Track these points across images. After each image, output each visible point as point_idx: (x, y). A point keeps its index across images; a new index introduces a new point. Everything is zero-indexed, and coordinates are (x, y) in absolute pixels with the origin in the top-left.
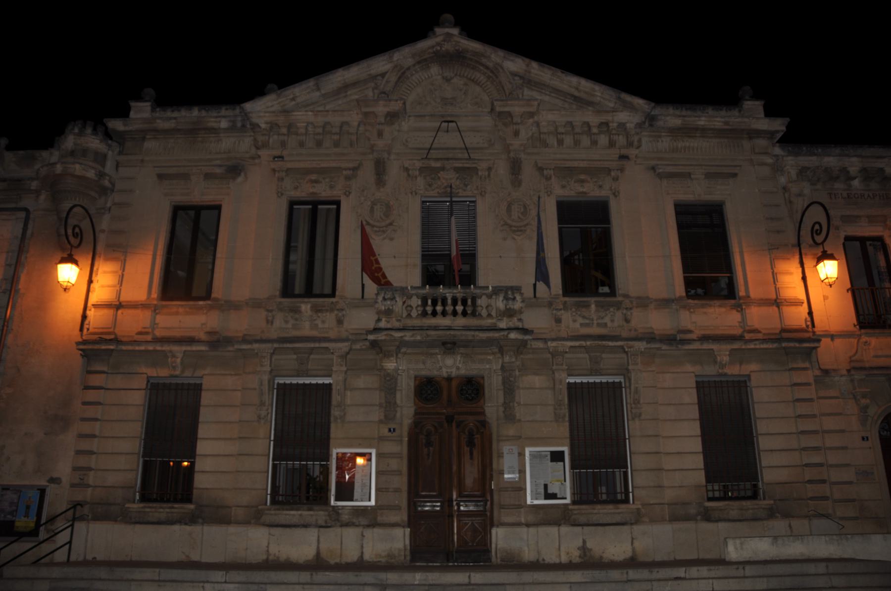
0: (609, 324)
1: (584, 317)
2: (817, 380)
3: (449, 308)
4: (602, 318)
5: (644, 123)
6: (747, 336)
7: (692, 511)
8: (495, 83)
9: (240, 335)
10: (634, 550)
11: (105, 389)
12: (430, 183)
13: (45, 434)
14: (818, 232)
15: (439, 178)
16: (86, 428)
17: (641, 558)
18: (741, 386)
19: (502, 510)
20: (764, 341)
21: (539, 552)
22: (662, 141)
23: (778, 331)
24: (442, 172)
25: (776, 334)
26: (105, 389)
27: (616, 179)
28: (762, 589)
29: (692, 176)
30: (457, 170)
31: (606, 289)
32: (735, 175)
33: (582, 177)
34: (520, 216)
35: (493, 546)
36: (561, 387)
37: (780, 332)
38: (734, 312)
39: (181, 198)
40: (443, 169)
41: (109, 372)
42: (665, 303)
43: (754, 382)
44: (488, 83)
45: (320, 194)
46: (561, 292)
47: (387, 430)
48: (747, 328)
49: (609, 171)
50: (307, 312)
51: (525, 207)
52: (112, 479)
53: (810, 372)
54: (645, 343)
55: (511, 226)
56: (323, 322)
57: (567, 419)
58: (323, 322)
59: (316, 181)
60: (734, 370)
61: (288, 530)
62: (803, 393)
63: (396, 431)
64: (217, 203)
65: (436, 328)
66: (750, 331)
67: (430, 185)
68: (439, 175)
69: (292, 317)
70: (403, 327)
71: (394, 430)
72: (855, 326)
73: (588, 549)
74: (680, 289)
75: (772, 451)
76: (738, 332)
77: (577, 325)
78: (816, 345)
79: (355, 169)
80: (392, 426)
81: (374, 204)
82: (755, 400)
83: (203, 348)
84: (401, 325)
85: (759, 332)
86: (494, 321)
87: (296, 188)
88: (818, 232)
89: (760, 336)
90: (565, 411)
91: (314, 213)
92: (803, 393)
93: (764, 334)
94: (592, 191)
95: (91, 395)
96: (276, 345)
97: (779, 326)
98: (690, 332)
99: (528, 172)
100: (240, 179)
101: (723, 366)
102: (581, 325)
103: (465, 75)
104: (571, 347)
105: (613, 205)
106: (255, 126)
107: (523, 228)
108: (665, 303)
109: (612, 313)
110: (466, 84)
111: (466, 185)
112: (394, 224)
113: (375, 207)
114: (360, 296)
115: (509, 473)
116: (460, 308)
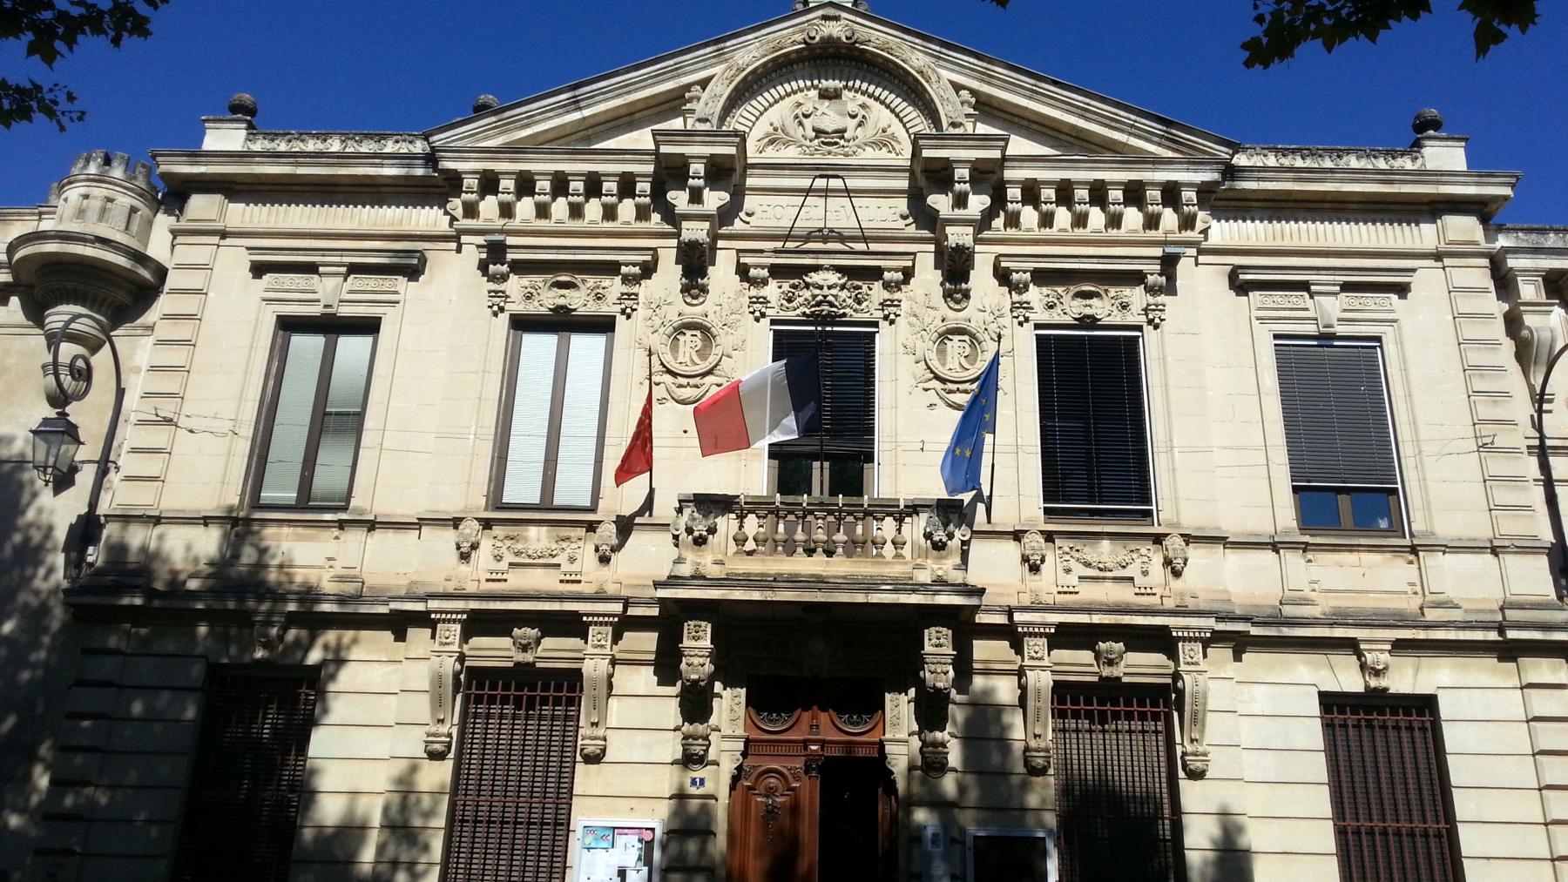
0: (1139, 580)
1: (1088, 565)
6: (1432, 615)
9: (404, 582)
12: (790, 294)
28: (1551, 577)
30: (838, 269)
31: (1383, 524)
37: (1502, 609)
40: (816, 268)
46: (1295, 524)
48: (1429, 598)
50: (539, 540)
58: (572, 560)
63: (689, 781)
67: (790, 300)
68: (807, 279)
70: (727, 574)
74: (1286, 516)
75: (1488, 858)
76: (1411, 604)
80: (698, 775)
84: (724, 573)
85: (1458, 607)
86: (907, 569)
89: (1456, 615)
91: (198, 292)
93: (1466, 611)
97: (1499, 596)
98: (1306, 602)
99: (981, 278)
109: (1145, 559)
110: (863, 106)
111: (859, 303)
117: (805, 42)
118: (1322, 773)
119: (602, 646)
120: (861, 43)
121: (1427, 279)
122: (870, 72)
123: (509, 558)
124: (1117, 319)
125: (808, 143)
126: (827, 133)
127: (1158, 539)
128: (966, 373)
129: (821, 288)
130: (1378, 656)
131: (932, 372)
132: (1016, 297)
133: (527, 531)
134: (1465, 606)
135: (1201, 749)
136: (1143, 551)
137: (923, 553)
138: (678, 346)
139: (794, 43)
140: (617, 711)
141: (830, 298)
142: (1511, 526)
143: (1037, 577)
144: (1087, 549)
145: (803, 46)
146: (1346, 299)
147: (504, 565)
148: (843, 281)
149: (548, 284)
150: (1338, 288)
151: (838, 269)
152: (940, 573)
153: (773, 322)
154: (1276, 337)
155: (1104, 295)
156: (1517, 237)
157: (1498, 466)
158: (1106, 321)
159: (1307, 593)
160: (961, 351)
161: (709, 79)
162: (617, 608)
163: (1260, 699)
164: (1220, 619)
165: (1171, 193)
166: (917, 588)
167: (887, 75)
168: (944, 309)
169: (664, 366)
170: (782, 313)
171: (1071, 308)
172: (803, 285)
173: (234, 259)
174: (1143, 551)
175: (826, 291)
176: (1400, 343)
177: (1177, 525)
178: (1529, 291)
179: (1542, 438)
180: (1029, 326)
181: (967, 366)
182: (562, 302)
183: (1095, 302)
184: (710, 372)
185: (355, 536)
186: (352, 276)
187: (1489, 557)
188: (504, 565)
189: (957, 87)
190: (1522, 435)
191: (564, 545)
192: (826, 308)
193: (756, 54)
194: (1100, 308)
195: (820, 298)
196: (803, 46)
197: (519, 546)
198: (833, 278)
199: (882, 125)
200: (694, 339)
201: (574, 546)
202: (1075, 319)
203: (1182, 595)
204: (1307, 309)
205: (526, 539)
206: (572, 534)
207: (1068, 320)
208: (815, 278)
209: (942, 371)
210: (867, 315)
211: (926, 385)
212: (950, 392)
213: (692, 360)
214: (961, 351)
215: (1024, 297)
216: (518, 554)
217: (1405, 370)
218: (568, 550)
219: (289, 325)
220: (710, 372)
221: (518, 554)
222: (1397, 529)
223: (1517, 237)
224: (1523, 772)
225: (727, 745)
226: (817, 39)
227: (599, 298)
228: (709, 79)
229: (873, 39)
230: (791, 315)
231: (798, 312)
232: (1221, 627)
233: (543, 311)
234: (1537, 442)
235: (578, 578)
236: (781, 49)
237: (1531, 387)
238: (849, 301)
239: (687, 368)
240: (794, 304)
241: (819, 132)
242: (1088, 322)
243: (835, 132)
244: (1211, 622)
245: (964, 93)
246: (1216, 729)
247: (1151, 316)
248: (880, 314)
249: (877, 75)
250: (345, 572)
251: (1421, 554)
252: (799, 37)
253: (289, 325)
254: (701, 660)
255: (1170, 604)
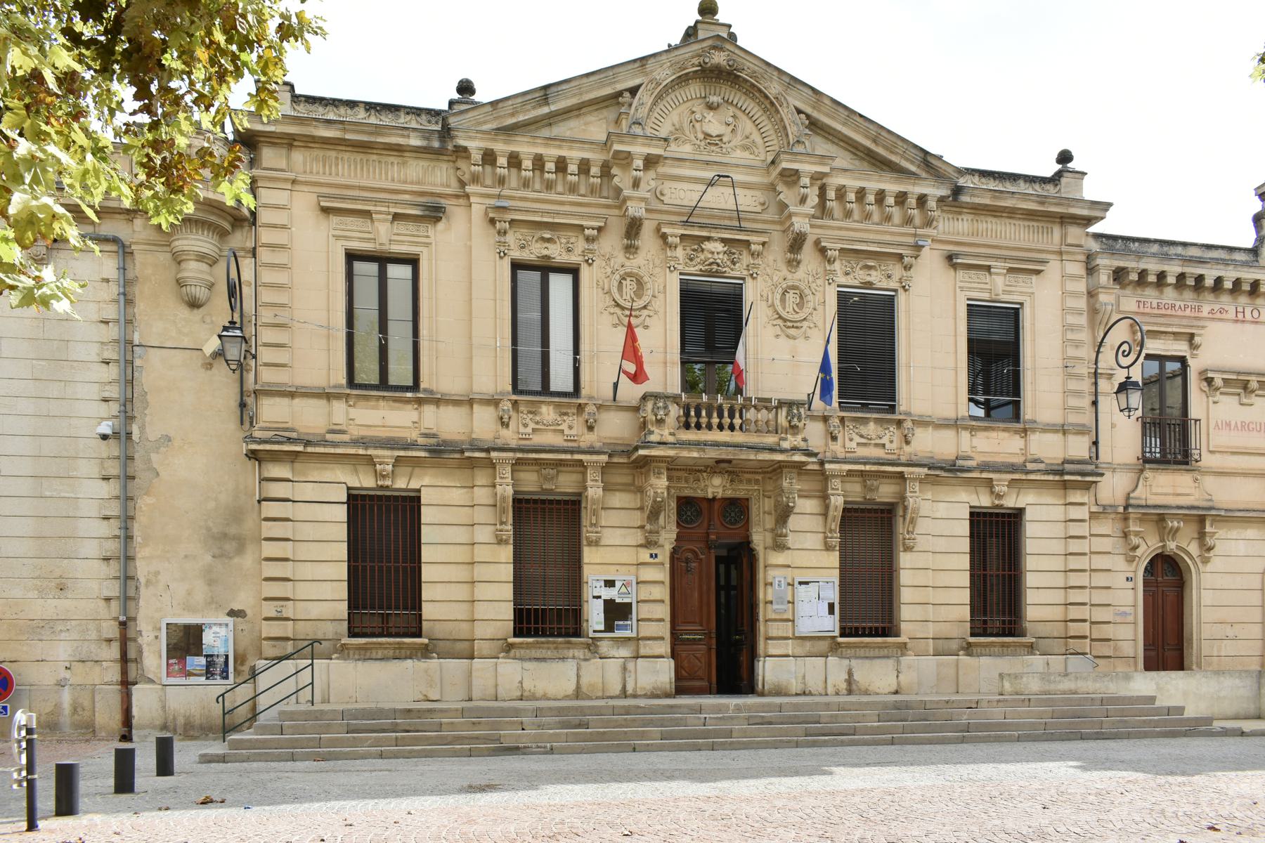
0: (567, 432)
1: (862, 436)
2: (1093, 515)
3: (727, 421)
4: (880, 438)
5: (949, 197)
6: (1030, 466)
7: (954, 645)
8: (773, 120)
10: (899, 684)
11: (294, 501)
13: (214, 557)
14: (1126, 353)
15: (703, 250)
16: (270, 549)
17: (549, 696)
18: (411, 504)
19: (769, 642)
20: (1047, 472)
21: (804, 683)
22: (962, 220)
23: (1060, 462)
24: (706, 243)
25: (1058, 464)
26: (294, 501)
27: (908, 268)
29: (992, 270)
30: (723, 241)
32: (1038, 272)
33: (871, 263)
34: (795, 306)
35: (760, 678)
36: (835, 514)
37: (1063, 463)
38: (1017, 437)
39: (982, 296)
40: (708, 239)
41: (294, 480)
42: (955, 424)
43: (1028, 515)
44: (763, 118)
45: (554, 258)
47: (649, 555)
48: (1029, 457)
49: (900, 257)
51: (801, 297)
52: (316, 611)
53: (1086, 508)
54: (926, 469)
55: (785, 320)
56: (570, 427)
57: (511, 542)
58: (570, 427)
59: (549, 240)
60: (1011, 502)
61: (543, 664)
62: (1075, 529)
64: (416, 257)
65: (716, 444)
66: (1035, 461)
67: (691, 260)
68: (703, 246)
69: (531, 419)
71: (656, 555)
72: (1138, 459)
73: (855, 680)
76: (1018, 460)
77: (854, 445)
78: (1098, 479)
79: (600, 229)
80: (654, 552)
81: (785, 292)
82: (1028, 535)
83: (423, 454)
85: (1042, 462)
87: (847, 274)
88: (1126, 353)
89: (1042, 466)
90: (835, 540)
91: (284, 227)
92: (1075, 529)
93: (1047, 464)
94: (881, 280)
95: (271, 509)
96: (519, 455)
98: (969, 458)
100: (441, 226)
101: (999, 496)
102: (858, 444)
103: (735, 103)
104: (850, 471)
105: (902, 301)
106: (462, 152)
107: (798, 324)
108: (955, 424)
109: (892, 433)
111: (734, 263)
112: (649, 307)
113: (787, 295)
114: (612, 398)
115: (778, 604)
116: (715, 420)
117: (701, 66)
118: (425, 530)
119: (596, 481)
120: (738, 71)
121: (1053, 269)
122: (740, 91)
123: (532, 425)
124: (884, 284)
125: (698, 142)
126: (712, 136)
127: (899, 423)
128: (796, 316)
129: (713, 253)
130: (1001, 488)
131: (778, 314)
132: (669, 254)
133: (541, 408)
134: (1046, 461)
135: (913, 537)
136: (891, 429)
137: (784, 431)
138: (785, 299)
139: (693, 65)
140: (606, 518)
141: (719, 261)
142: (1073, 418)
143: (908, 447)
144: (862, 427)
145: (699, 68)
146: (1011, 278)
147: (529, 430)
148: (725, 249)
149: (535, 239)
150: (1005, 271)
151: (723, 241)
152: (795, 443)
153: (681, 274)
154: (968, 299)
155: (557, 240)
156: (1102, 241)
157: (1073, 385)
158: (879, 285)
159: (970, 453)
160: (631, 287)
161: (638, 87)
162: (604, 458)
163: (942, 510)
164: (929, 468)
165: (922, 200)
166: (782, 451)
167: (751, 95)
168: (785, 271)
169: (616, 302)
170: (687, 268)
171: (861, 276)
172: (700, 250)
173: (303, 204)
174: (891, 429)
175: (716, 256)
176: (1033, 307)
177: (909, 414)
178: (1104, 278)
179: (1096, 369)
180: (834, 286)
181: (798, 310)
182: (545, 252)
183: (873, 273)
184: (645, 307)
185: (429, 410)
186: (396, 222)
187: (1060, 435)
188: (529, 430)
189: (799, 112)
190: (1085, 370)
191: (565, 418)
192: (715, 267)
193: (668, 72)
194: (875, 277)
195: (711, 260)
196: (699, 68)
197: (538, 418)
198: (719, 247)
199: (747, 133)
200: (632, 283)
201: (571, 418)
202: (538, 257)
203: (910, 454)
204: (987, 283)
205: (541, 414)
206: (569, 411)
207: (856, 283)
208: (708, 245)
209: (784, 314)
210: (739, 273)
211: (775, 323)
212: (789, 327)
213: (795, 311)
214: (794, 300)
215: (832, 268)
216: (537, 423)
217: (1033, 324)
218: (567, 421)
219: (352, 257)
220: (645, 307)
221: (537, 423)
222: (1017, 417)
223: (1102, 241)
224: (1058, 547)
225: (667, 536)
226: (709, 65)
227: (889, 277)
228: (638, 87)
229: (746, 68)
230: (692, 270)
231: (697, 268)
232: (930, 472)
233: (533, 257)
234: (1093, 371)
235: (576, 438)
236: (684, 69)
237: (1094, 338)
238: (728, 263)
239: (791, 316)
240: (694, 263)
241: (707, 135)
242: (869, 285)
243: (717, 136)
244: (925, 470)
245: (803, 116)
246: (923, 526)
247: (904, 284)
248: (745, 273)
249: (745, 93)
250: (427, 431)
251: (1028, 433)
252: (696, 61)
253: (352, 257)
254: (662, 491)
255: (903, 459)
